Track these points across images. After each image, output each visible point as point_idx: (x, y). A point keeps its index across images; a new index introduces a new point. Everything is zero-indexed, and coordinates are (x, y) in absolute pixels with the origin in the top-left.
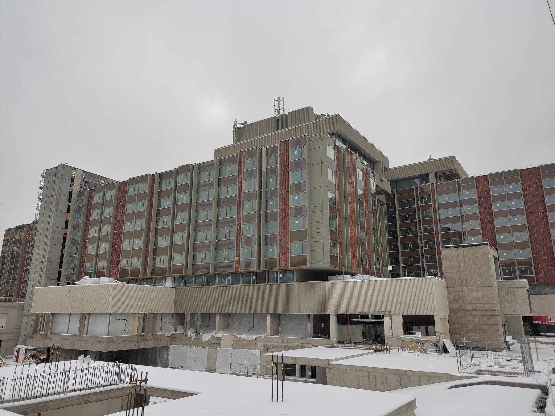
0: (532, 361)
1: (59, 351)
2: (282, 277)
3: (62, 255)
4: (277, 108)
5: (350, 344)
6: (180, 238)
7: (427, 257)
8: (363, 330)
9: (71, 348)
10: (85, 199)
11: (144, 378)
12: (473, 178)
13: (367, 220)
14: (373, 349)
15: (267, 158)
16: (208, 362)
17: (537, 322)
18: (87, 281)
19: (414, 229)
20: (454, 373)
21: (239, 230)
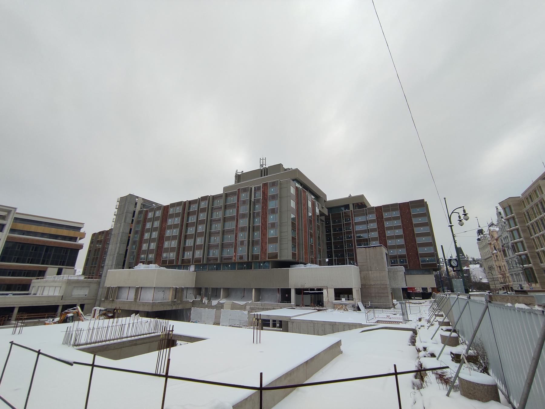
0: (407, 314)
1: (120, 311)
2: (262, 266)
3: (127, 250)
4: (262, 164)
5: (303, 306)
6: (200, 241)
7: (348, 253)
8: (311, 298)
9: (129, 309)
10: (142, 216)
11: (171, 329)
12: (374, 207)
13: (314, 231)
14: (316, 310)
15: (255, 193)
16: (215, 318)
17: (410, 291)
18: (141, 267)
19: (341, 237)
20: (364, 323)
21: (236, 236)
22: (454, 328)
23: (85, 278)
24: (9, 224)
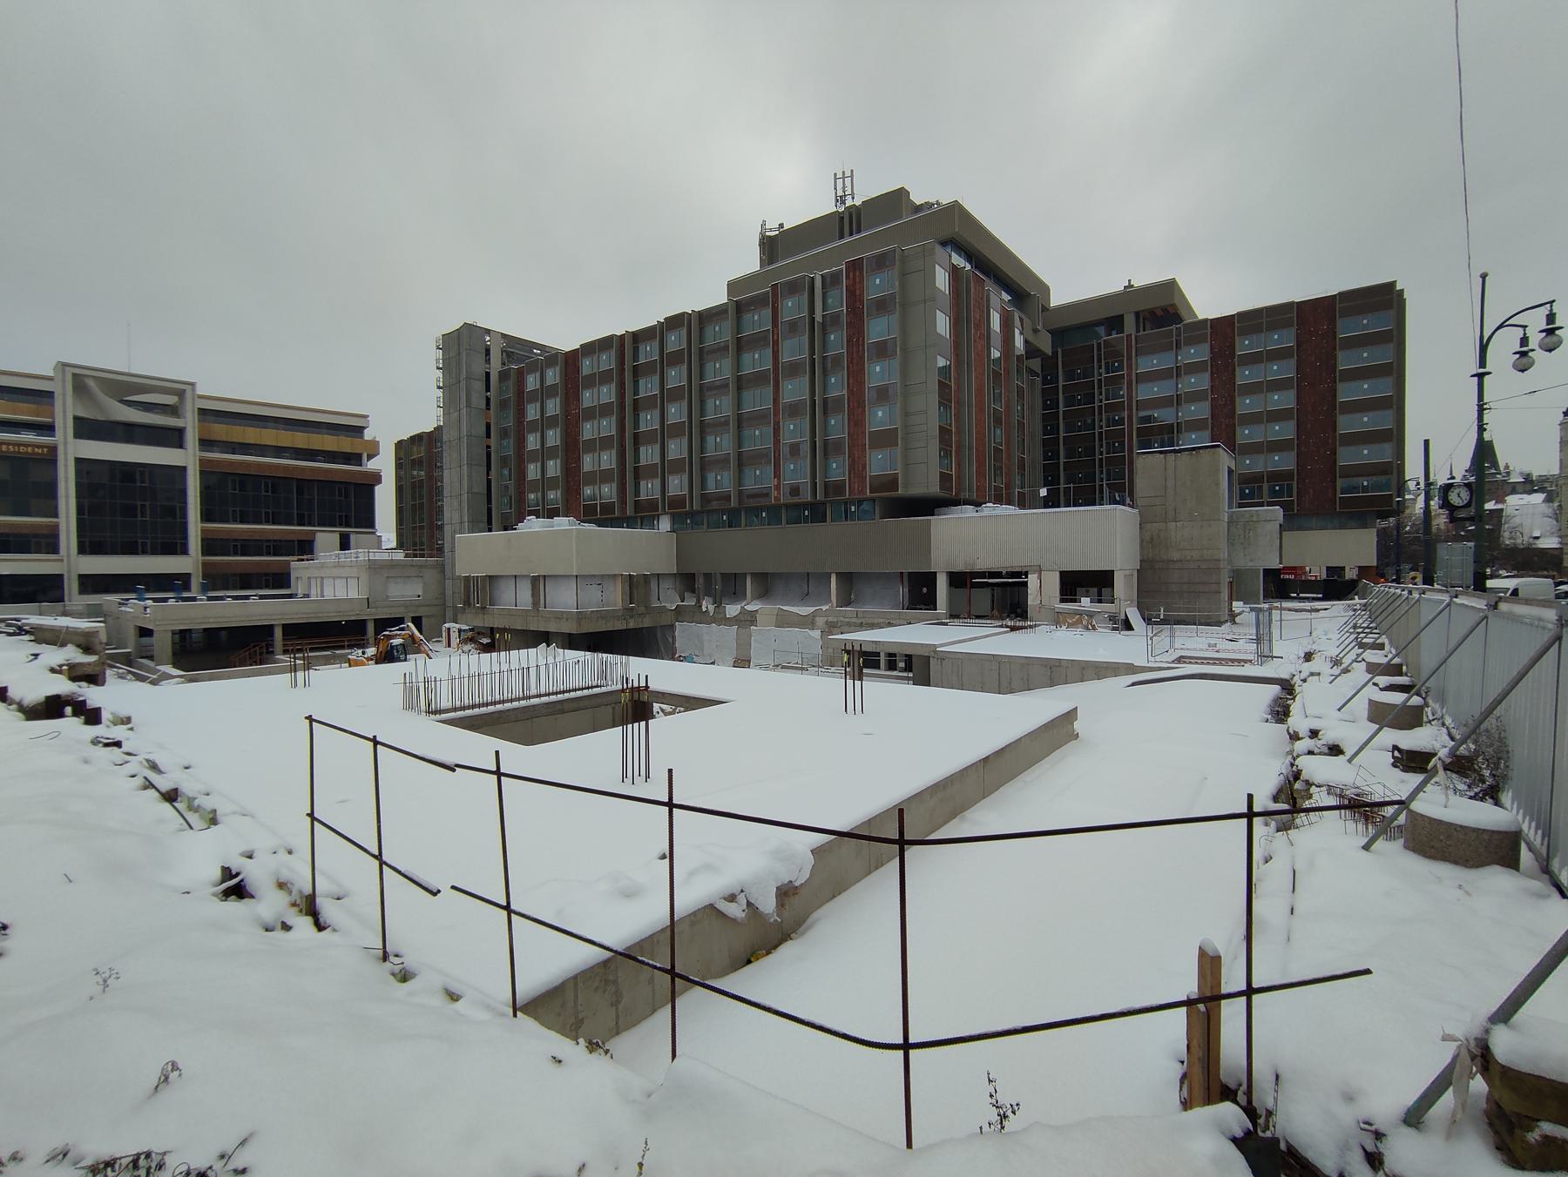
4: (840, 193)
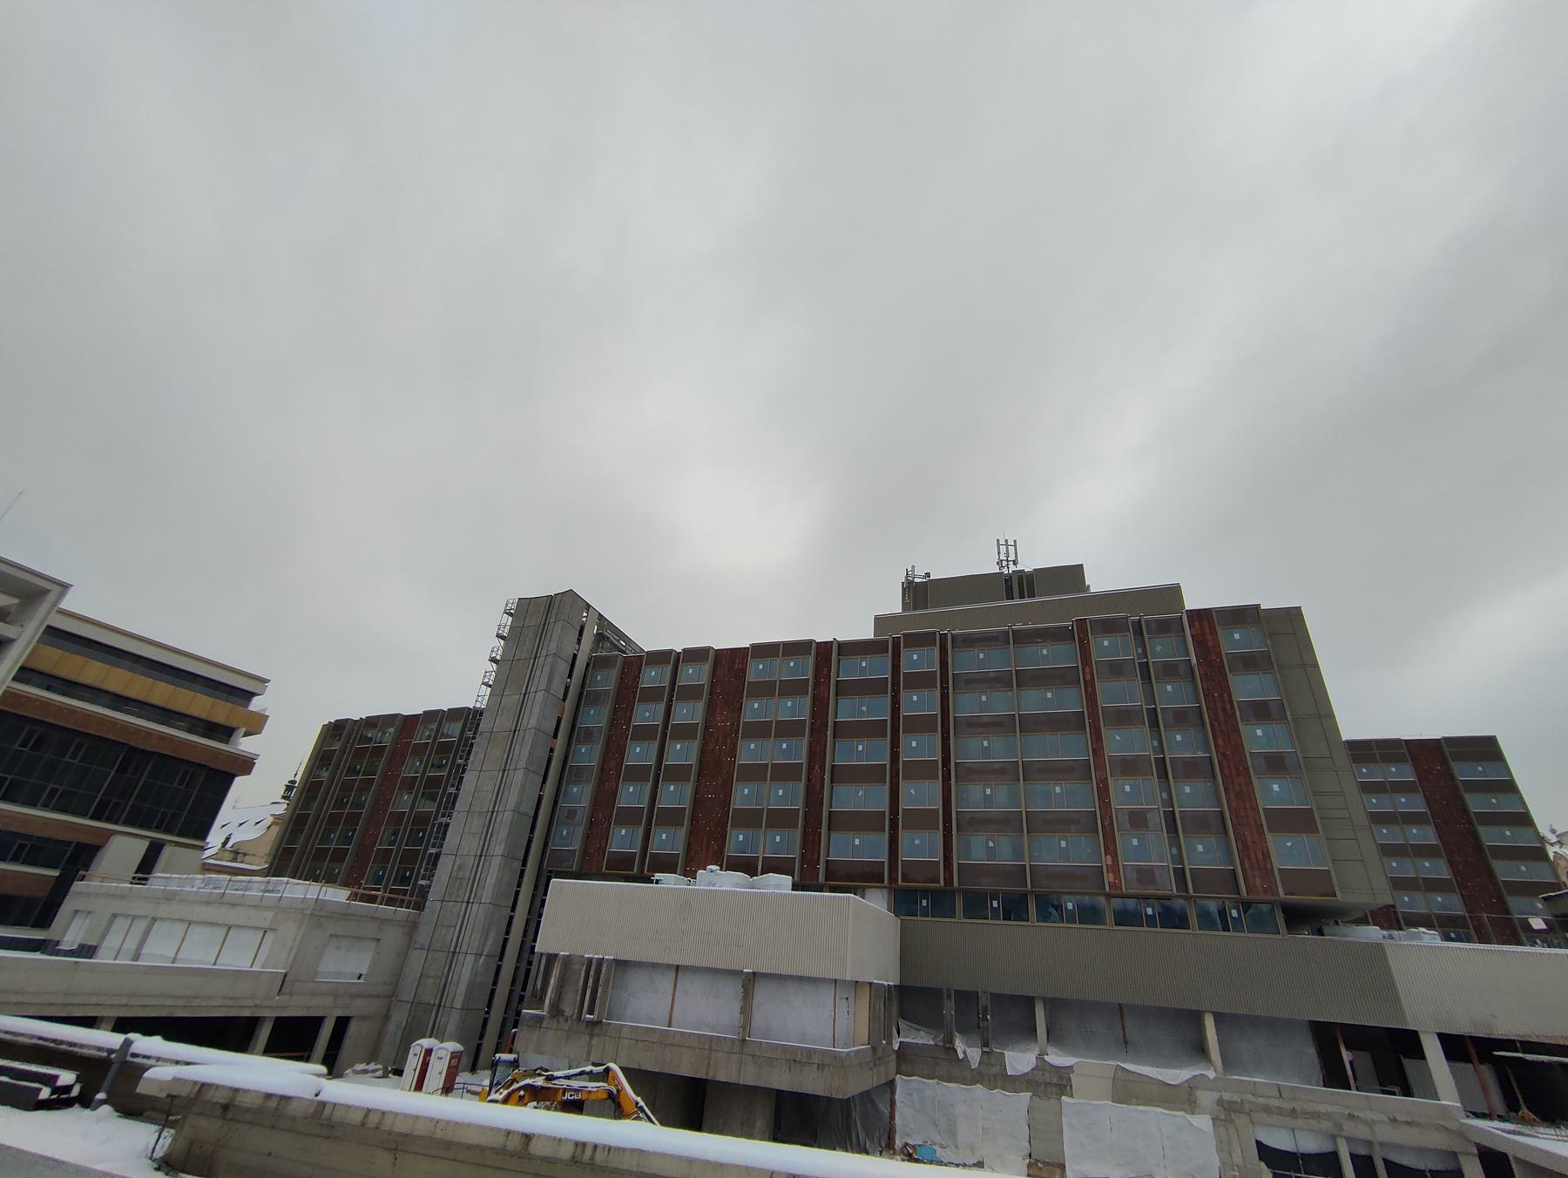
3: (540, 798)
4: (1003, 557)
18: (717, 880)
22: (1461, 1153)
23: (354, 896)
24: (25, 639)
